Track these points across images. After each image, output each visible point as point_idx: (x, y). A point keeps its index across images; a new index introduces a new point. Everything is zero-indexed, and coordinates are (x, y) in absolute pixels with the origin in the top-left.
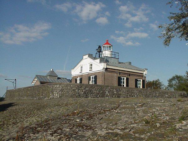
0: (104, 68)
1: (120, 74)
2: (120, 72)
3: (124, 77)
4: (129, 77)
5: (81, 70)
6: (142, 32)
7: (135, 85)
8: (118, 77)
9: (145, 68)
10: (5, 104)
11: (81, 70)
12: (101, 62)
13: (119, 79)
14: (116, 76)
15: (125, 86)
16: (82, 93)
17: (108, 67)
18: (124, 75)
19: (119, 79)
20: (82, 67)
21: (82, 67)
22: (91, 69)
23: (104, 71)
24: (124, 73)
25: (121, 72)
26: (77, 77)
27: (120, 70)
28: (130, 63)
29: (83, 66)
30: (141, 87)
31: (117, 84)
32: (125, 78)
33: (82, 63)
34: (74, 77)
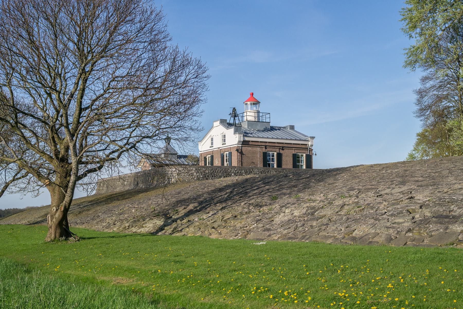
0: (239, 142)
1: (266, 148)
2: (266, 145)
3: (273, 153)
4: (281, 152)
5: (212, 144)
6: (79, 229)
7: (292, 163)
8: (264, 153)
9: (13, 195)
10: (60, 221)
11: (212, 144)
12: (235, 132)
13: (280, 156)
14: (259, 151)
15: (275, 167)
16: (202, 176)
17: (247, 139)
18: (274, 150)
19: (265, 155)
20: (212, 139)
21: (212, 139)
22: (224, 143)
23: (241, 145)
24: (273, 146)
25: (267, 144)
26: (208, 153)
27: (266, 142)
28: (292, 127)
29: (214, 137)
30: (304, 167)
31: (262, 163)
32: (275, 154)
33: (212, 133)
34: (201, 154)
